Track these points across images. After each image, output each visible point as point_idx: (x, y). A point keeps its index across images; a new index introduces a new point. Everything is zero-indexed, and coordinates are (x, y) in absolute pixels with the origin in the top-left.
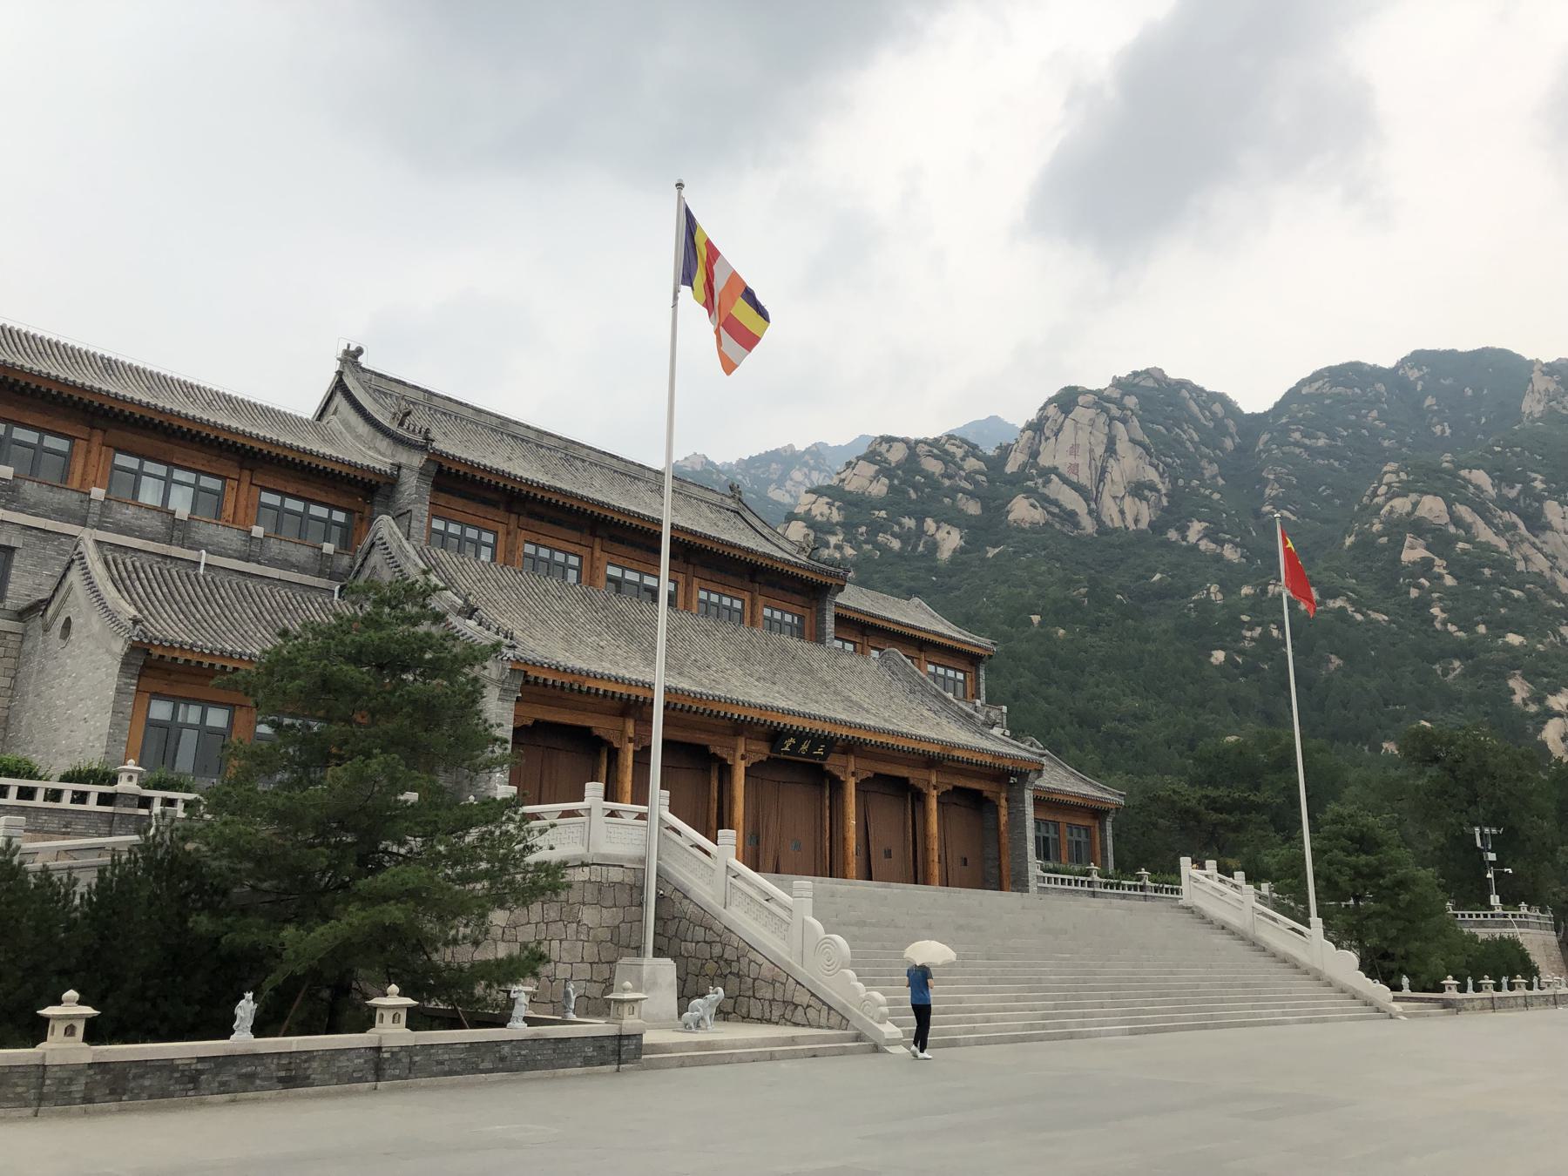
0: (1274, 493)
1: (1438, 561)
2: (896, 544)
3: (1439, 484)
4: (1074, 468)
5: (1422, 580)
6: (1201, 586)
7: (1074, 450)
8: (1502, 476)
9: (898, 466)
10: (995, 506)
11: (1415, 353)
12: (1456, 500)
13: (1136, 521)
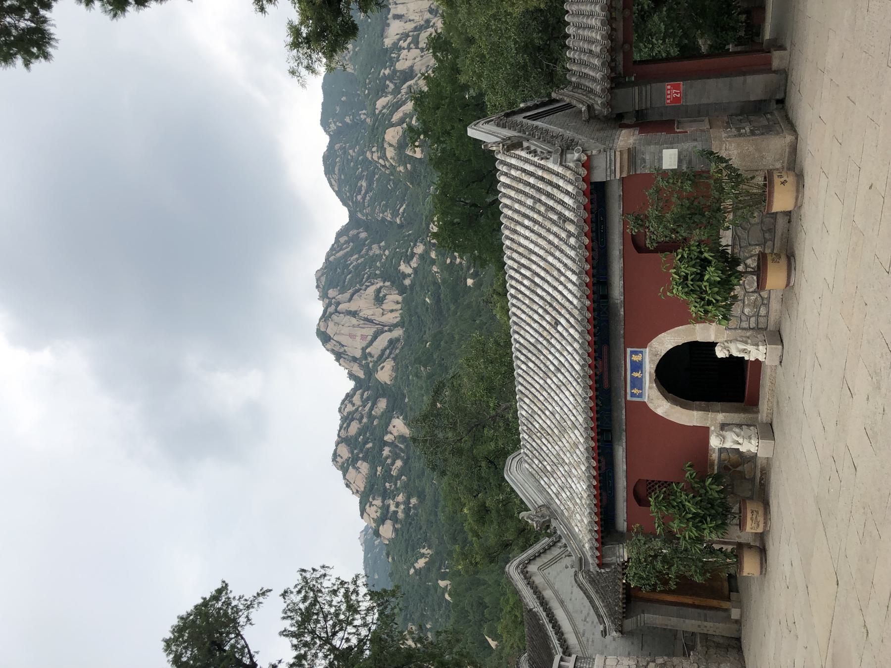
2: (399, 463)
3: (380, 129)
4: (363, 337)
6: (434, 276)
8: (381, 91)
9: (352, 453)
10: (381, 390)
11: (322, 124)
12: (389, 121)
13: (398, 303)
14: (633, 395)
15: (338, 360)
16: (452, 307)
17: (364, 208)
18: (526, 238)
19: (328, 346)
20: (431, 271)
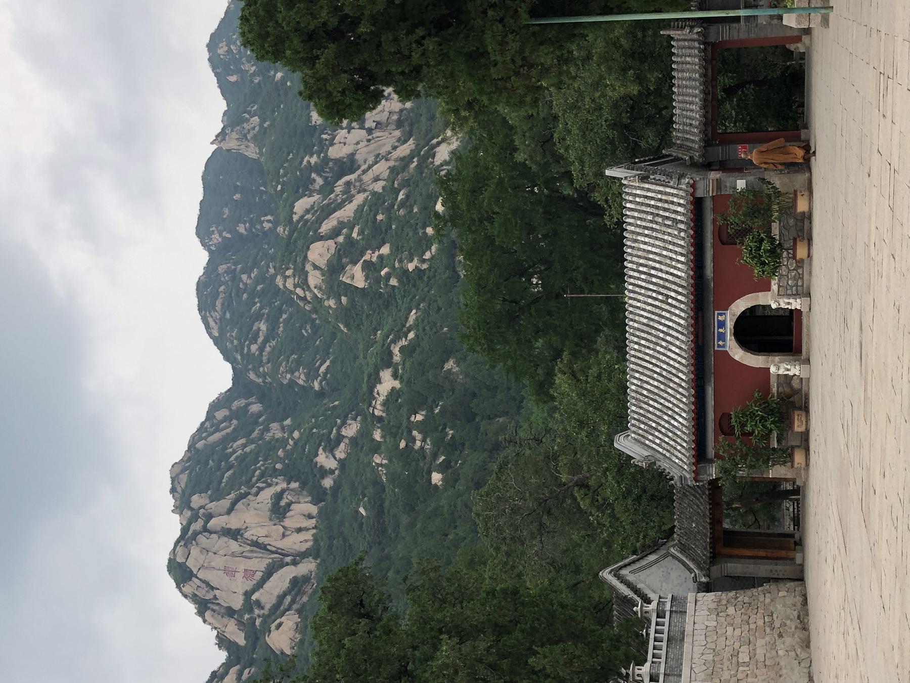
0: (302, 377)
1: (367, 257)
3: (300, 243)
4: (249, 574)
5: (383, 273)
6: (374, 471)
7: (229, 572)
8: (302, 187)
12: (316, 231)
13: (310, 517)
14: (719, 346)
15: (201, 613)
16: (405, 520)
17: (261, 364)
18: (645, 243)
19: (187, 589)
20: (370, 463)
